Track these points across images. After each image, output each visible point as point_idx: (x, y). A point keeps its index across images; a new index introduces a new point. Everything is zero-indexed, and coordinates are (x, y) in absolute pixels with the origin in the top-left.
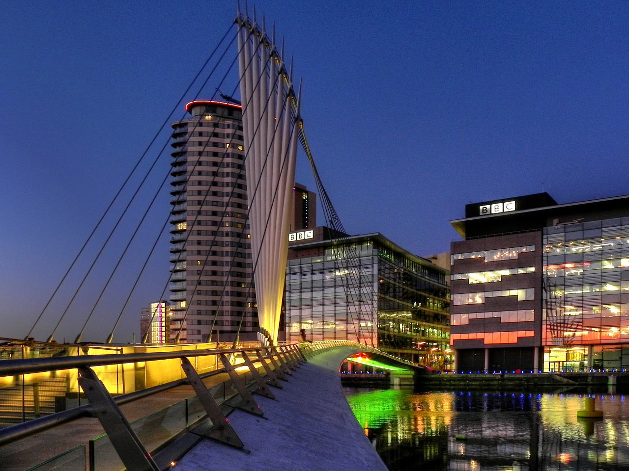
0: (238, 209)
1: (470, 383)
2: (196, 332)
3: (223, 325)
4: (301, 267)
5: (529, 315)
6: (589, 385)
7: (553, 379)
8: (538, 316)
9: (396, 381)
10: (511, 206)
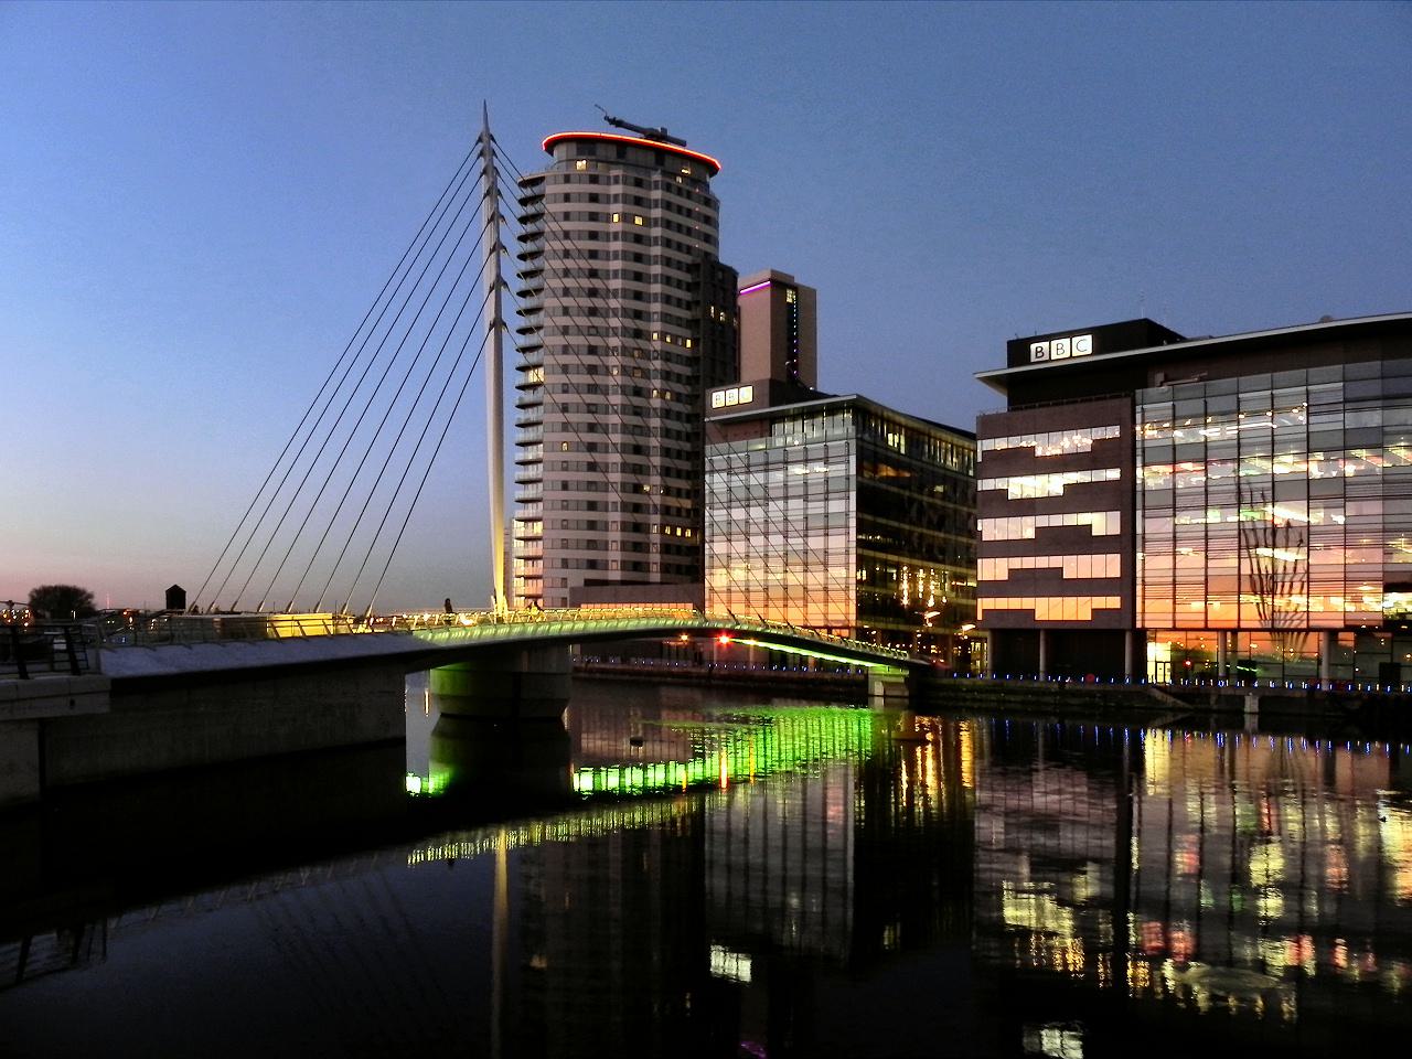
1: (1007, 698)
2: (559, 582)
3: (607, 569)
4: (806, 449)
5: (1108, 566)
6: (1210, 711)
7: (1149, 696)
8: (1129, 566)
9: (878, 689)
10: (1084, 345)
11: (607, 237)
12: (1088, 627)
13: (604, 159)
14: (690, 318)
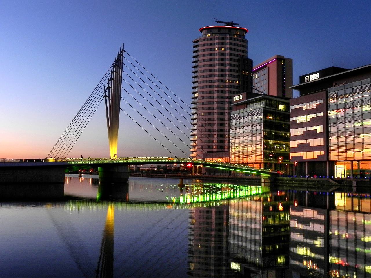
0: (221, 83)
5: (320, 142)
6: (344, 186)
7: (329, 182)
8: (327, 142)
9: (263, 181)
10: (317, 76)
11: (214, 55)
12: (316, 161)
13: (214, 33)
14: (237, 75)
